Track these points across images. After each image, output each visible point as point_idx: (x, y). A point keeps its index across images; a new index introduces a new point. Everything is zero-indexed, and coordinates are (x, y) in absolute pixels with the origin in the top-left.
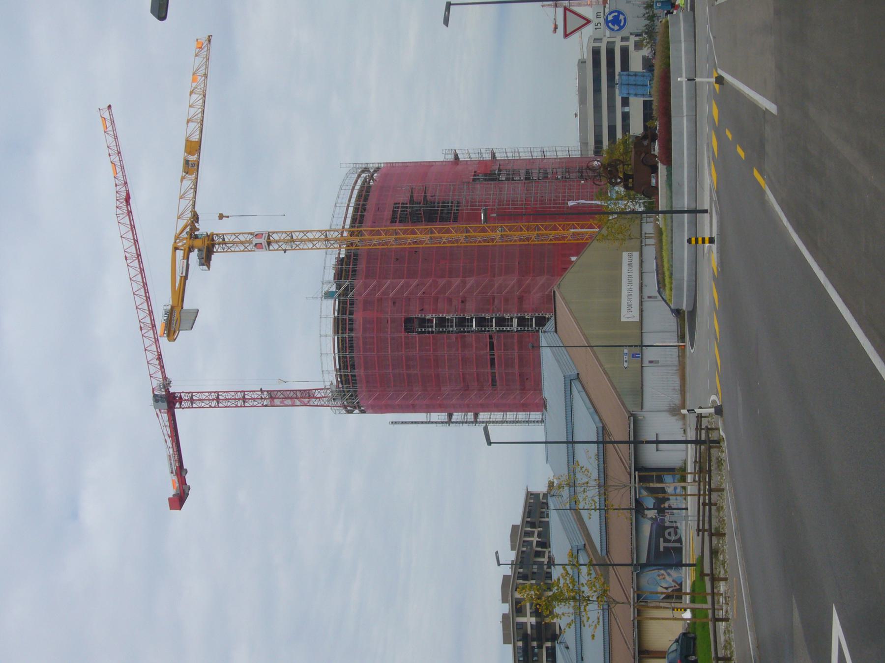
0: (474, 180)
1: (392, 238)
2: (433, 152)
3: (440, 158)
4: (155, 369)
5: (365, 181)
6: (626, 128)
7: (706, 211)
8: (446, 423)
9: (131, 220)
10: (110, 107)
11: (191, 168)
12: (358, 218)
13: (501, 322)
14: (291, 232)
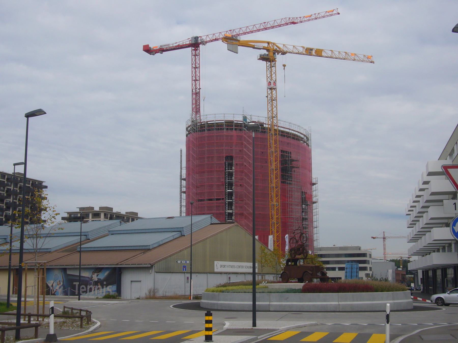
0: (302, 192)
1: (273, 150)
2: (316, 174)
3: (314, 176)
4: (211, 37)
5: (302, 138)
6: (328, 269)
7: (254, 324)
8: (181, 177)
9: (283, 25)
10: (339, 14)
11: (309, 52)
12: (284, 134)
13: (230, 204)
14: (276, 100)
